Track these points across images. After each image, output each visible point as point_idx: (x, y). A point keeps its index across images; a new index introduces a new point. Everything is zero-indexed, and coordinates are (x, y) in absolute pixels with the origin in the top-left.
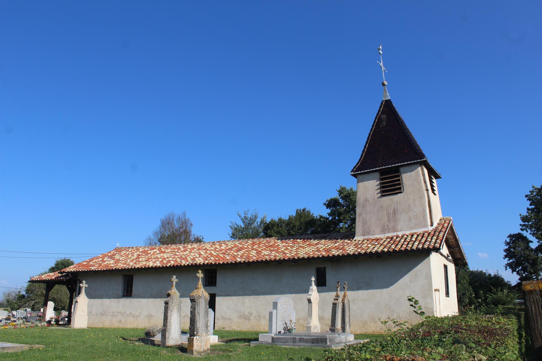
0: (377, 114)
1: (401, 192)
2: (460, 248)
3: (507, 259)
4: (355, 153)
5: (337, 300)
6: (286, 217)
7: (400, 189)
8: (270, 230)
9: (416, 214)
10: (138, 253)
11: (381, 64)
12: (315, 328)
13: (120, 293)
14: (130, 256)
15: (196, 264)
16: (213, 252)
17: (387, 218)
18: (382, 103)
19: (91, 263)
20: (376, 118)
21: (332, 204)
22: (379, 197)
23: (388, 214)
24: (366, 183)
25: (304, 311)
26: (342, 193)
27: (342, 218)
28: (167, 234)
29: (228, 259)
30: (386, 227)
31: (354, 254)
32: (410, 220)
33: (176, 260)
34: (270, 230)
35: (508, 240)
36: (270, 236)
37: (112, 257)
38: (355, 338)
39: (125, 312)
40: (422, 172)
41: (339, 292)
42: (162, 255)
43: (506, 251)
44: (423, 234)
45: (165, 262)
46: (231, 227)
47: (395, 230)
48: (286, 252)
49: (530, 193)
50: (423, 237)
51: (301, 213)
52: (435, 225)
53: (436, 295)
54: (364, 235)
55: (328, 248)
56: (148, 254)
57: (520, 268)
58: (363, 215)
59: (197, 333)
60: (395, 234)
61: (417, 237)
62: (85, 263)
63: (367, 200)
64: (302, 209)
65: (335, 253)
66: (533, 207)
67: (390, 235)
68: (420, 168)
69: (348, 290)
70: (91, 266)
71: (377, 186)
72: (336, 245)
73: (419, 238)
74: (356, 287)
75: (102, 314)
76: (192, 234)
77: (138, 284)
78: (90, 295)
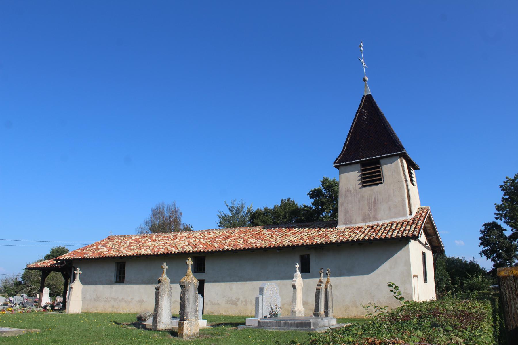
0: (359, 109)
1: (381, 183)
2: (437, 236)
3: (482, 246)
4: (337, 148)
5: (321, 285)
6: (271, 207)
7: (380, 179)
8: (257, 219)
9: (395, 204)
10: (130, 241)
11: (363, 61)
12: (299, 312)
13: (113, 279)
14: (122, 244)
15: (185, 252)
16: (201, 240)
17: (368, 208)
18: (363, 98)
19: (85, 251)
20: (357, 112)
21: (315, 194)
22: (360, 188)
23: (369, 203)
24: (348, 174)
25: (288, 296)
26: (325, 184)
27: (325, 207)
28: (157, 223)
29: (217, 246)
30: (367, 216)
31: (336, 242)
32: (390, 209)
33: (166, 248)
34: (257, 219)
35: (483, 229)
36: (256, 225)
37: (105, 245)
38: (338, 322)
39: (118, 298)
40: (401, 164)
41: (322, 278)
42: (153, 243)
43: (481, 238)
44: (403, 223)
45: (156, 250)
46: (219, 216)
47: (375, 219)
48: (272, 240)
49: (504, 184)
50: (402, 226)
51: (286, 203)
52: (414, 214)
53: (414, 281)
54: (346, 224)
55: (312, 236)
56: (140, 242)
57: (495, 255)
58: (346, 205)
59: (187, 317)
60: (376, 223)
61: (396, 226)
62: (79, 251)
63: (348, 191)
64: (287, 199)
65: (318, 240)
66: (507, 197)
67: (371, 223)
68: (399, 160)
69: (330, 276)
70: (85, 253)
71: (359, 177)
72: (320, 233)
73: (399, 226)
74: (351, 272)
75: (95, 300)
76: (182, 223)
77: (130, 271)
78: (84, 282)
